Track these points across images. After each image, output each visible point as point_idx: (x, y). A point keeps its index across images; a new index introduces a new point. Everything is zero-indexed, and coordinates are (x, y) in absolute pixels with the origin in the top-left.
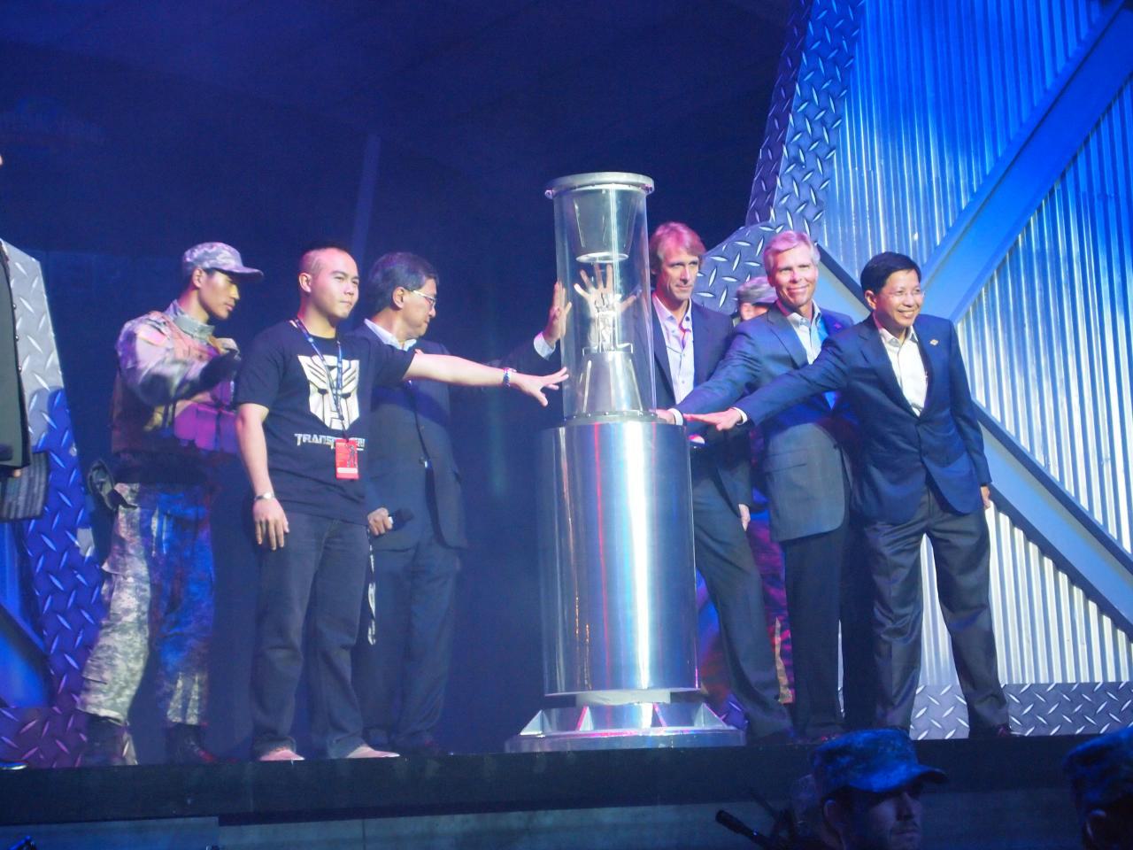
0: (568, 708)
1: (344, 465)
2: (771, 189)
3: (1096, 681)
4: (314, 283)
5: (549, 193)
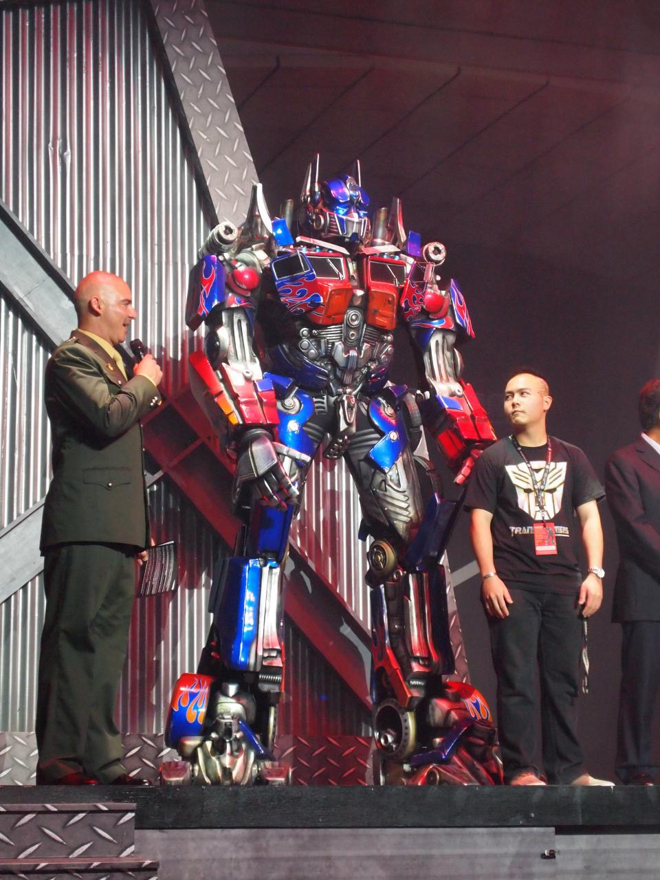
1: (542, 544)
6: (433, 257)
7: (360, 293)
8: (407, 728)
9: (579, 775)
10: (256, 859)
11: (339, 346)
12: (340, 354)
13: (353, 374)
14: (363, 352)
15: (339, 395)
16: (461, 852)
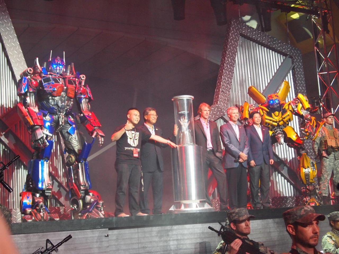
0: (179, 206)
1: (135, 154)
2: (218, 97)
3: (287, 196)
4: (130, 116)
5: (172, 100)
6: (82, 78)
7: (65, 88)
8: (80, 204)
9: (138, 213)
10: (27, 242)
11: (60, 102)
12: (60, 104)
13: (63, 110)
14: (66, 103)
15: (59, 115)
16: (83, 236)
